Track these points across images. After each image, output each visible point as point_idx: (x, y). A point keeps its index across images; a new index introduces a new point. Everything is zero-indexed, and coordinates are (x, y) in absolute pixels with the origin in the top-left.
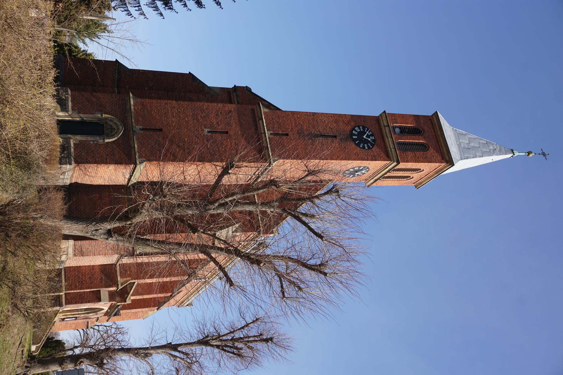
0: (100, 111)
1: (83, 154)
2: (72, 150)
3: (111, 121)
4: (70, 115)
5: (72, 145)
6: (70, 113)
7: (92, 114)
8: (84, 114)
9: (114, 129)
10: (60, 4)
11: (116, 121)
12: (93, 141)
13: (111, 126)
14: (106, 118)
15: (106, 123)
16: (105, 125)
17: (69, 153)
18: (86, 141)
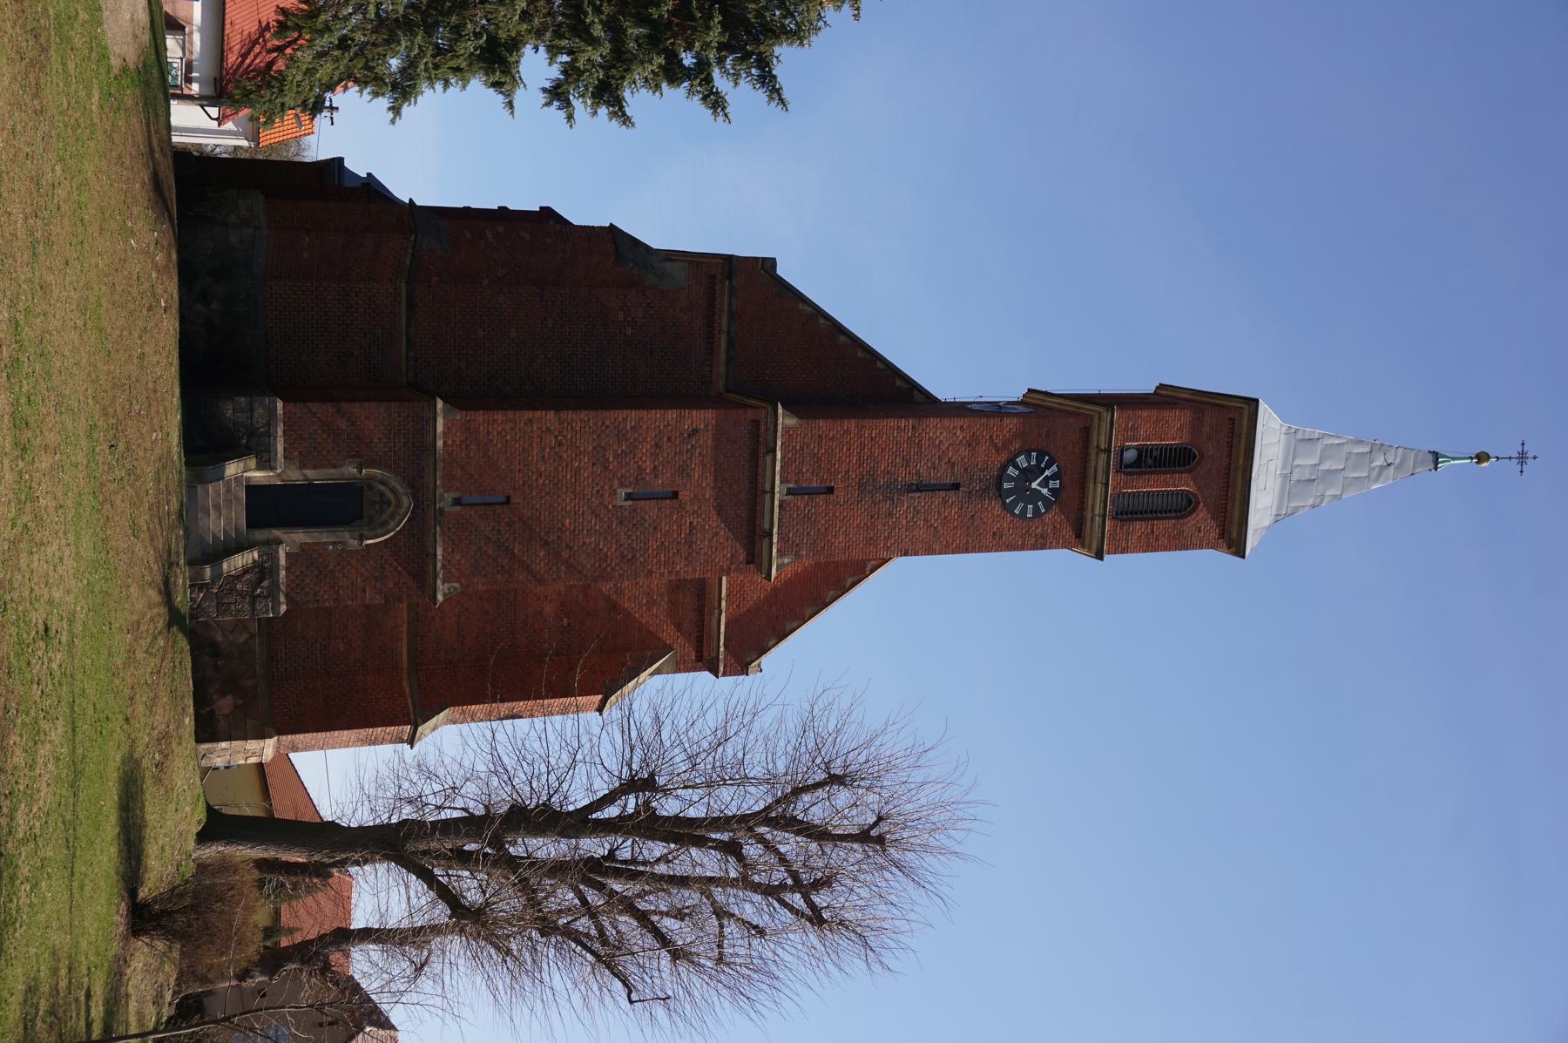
0: (357, 456)
2: (283, 573)
3: (382, 482)
5: (283, 561)
8: (315, 468)
9: (389, 503)
13: (382, 494)
14: (371, 478)
15: (370, 487)
18: (316, 544)
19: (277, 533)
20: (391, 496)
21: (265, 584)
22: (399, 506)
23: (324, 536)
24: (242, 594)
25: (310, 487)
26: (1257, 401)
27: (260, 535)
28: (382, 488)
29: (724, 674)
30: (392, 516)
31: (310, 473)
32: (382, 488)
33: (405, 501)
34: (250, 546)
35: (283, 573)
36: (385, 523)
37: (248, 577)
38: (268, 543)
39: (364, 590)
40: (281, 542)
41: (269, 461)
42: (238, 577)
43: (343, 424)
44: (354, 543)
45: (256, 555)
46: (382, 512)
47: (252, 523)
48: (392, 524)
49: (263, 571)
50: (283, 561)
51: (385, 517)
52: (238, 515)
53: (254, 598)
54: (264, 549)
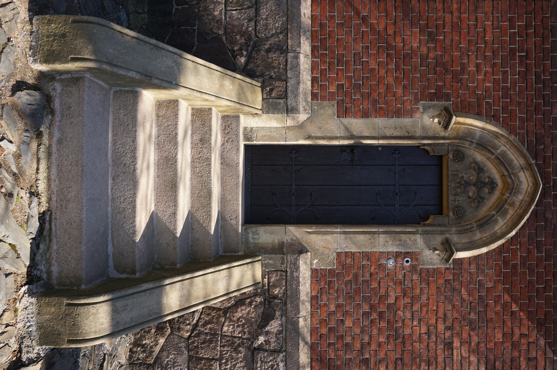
0: (438, 95)
1: (348, 323)
2: (305, 309)
3: (483, 145)
4: (301, 126)
5: (305, 288)
6: (303, 117)
7: (398, 114)
8: (365, 115)
9: (492, 185)
10: (101, 109)
11: (503, 147)
12: (397, 255)
13: (480, 169)
14: (467, 136)
15: (459, 155)
16: (451, 167)
17: (291, 330)
18: (367, 256)
19: (296, 232)
20: (494, 172)
21: (274, 326)
22: (512, 188)
23: (379, 242)
24: (232, 344)
25: (356, 153)
26: (177, 101)
27: (268, 235)
28: (479, 157)
29: (312, 61)
30: (500, 208)
31: (358, 125)
32: (479, 157)
33: (525, 180)
34: (250, 253)
35: (305, 309)
36: (485, 223)
37: (241, 312)
38: (280, 249)
39: (449, 346)
40: (301, 250)
41: (284, 96)
42: (226, 311)
43: (414, 40)
44: (432, 258)
45: (258, 270)
46: (480, 200)
47: (255, 215)
48: (500, 224)
49: (270, 301)
50: (305, 288)
51: (484, 211)
52: (225, 196)
53: (254, 351)
54: (274, 260)
